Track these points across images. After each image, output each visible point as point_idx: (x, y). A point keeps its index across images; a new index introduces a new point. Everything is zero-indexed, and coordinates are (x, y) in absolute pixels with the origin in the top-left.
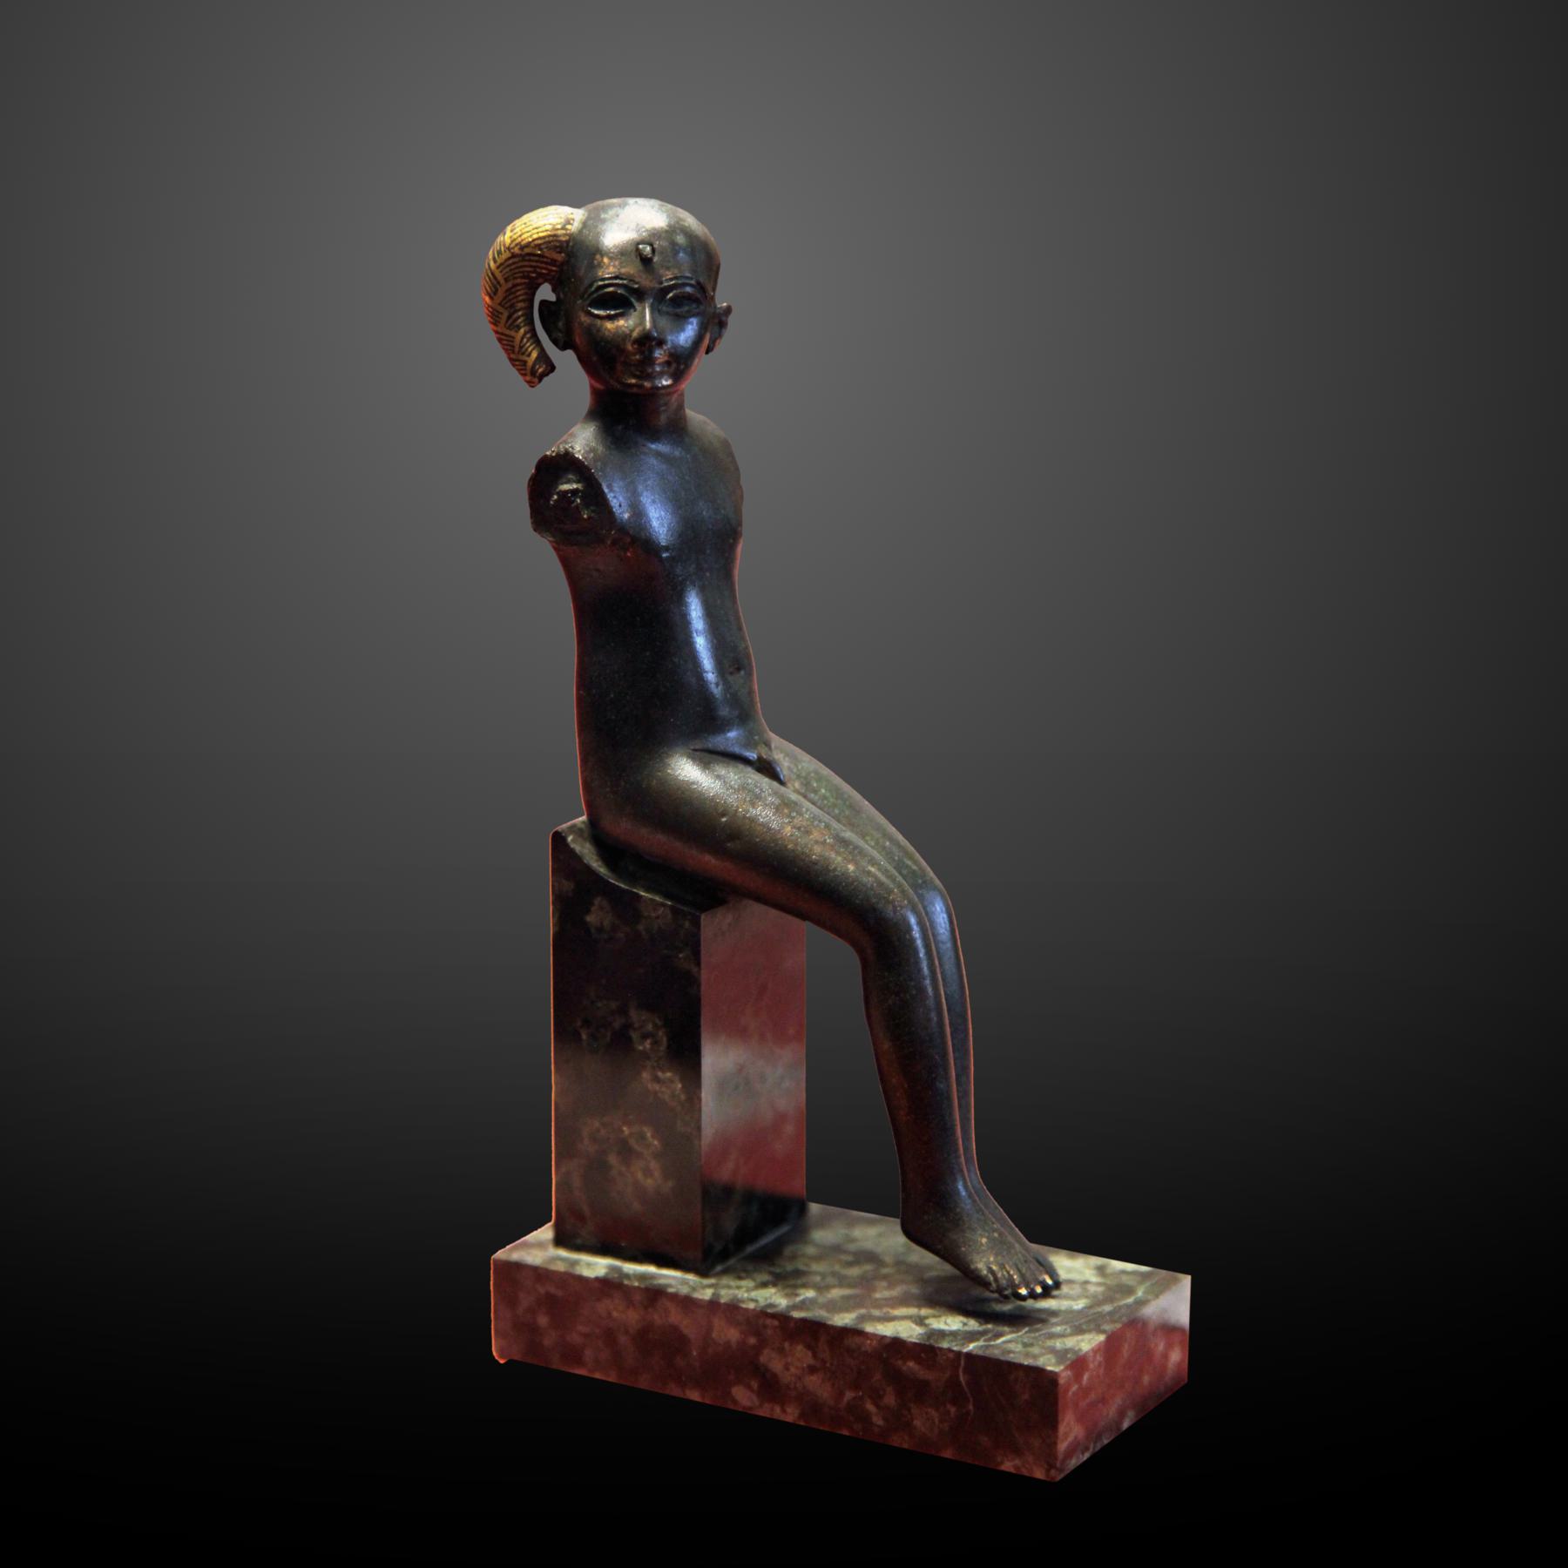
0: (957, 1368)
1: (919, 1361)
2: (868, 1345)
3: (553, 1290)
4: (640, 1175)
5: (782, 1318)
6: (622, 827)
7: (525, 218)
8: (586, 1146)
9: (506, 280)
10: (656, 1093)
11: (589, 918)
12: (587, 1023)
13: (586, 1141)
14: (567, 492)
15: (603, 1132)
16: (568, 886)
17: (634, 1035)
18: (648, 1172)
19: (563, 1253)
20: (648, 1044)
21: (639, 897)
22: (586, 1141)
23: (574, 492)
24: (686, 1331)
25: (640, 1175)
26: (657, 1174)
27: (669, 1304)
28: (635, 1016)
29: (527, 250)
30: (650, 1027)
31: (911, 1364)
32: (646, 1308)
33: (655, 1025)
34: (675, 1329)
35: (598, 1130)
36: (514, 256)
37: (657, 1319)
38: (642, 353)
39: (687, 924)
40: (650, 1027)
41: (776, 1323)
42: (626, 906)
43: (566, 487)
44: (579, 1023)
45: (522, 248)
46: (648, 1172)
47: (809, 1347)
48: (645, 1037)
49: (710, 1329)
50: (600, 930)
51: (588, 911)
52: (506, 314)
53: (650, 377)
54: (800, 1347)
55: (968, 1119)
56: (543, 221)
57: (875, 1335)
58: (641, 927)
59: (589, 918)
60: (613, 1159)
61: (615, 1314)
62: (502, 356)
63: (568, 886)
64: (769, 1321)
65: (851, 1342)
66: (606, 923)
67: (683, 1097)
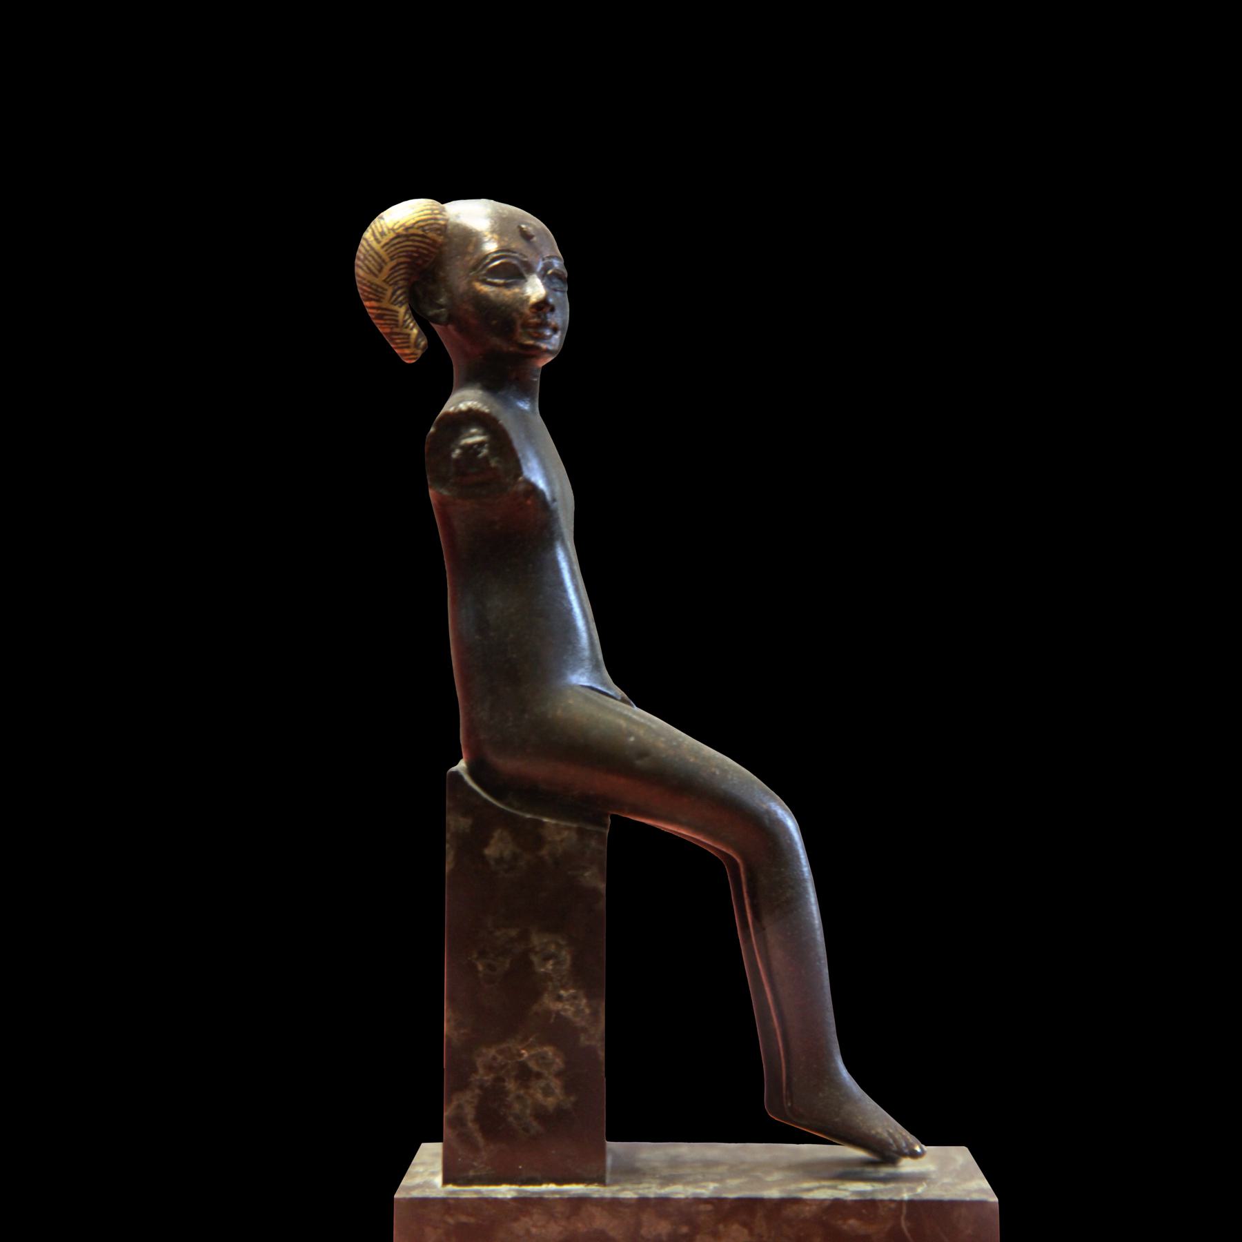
0: (898, 1217)
1: (860, 1217)
2: (807, 1211)
3: (463, 1219)
4: (539, 1096)
5: (717, 1203)
9: (392, 259)
10: (558, 1013)
11: (487, 852)
12: (482, 954)
13: (481, 1071)
14: (471, 446)
15: (500, 1058)
17: (535, 959)
18: (547, 1091)
20: (550, 965)
21: (543, 823)
22: (481, 1071)
23: (481, 444)
24: (612, 1234)
25: (539, 1096)
26: (558, 1091)
27: (594, 1210)
28: (536, 940)
29: (411, 231)
30: (552, 948)
31: (852, 1222)
32: (568, 1218)
33: (558, 945)
34: (602, 1232)
35: (494, 1058)
36: (398, 236)
37: (581, 1227)
38: (539, 317)
40: (552, 948)
41: (709, 1207)
42: (530, 837)
43: (470, 441)
44: (475, 956)
45: (407, 229)
46: (547, 1091)
47: (745, 1225)
48: (546, 959)
49: (639, 1224)
50: (500, 860)
51: (486, 844)
52: (389, 293)
53: (542, 338)
54: (735, 1227)
55: (778, 1017)
57: (814, 1200)
58: (544, 852)
59: (487, 852)
60: (511, 1085)
61: (534, 1230)
64: (702, 1207)
65: (789, 1212)
66: (507, 853)
67: (587, 1011)
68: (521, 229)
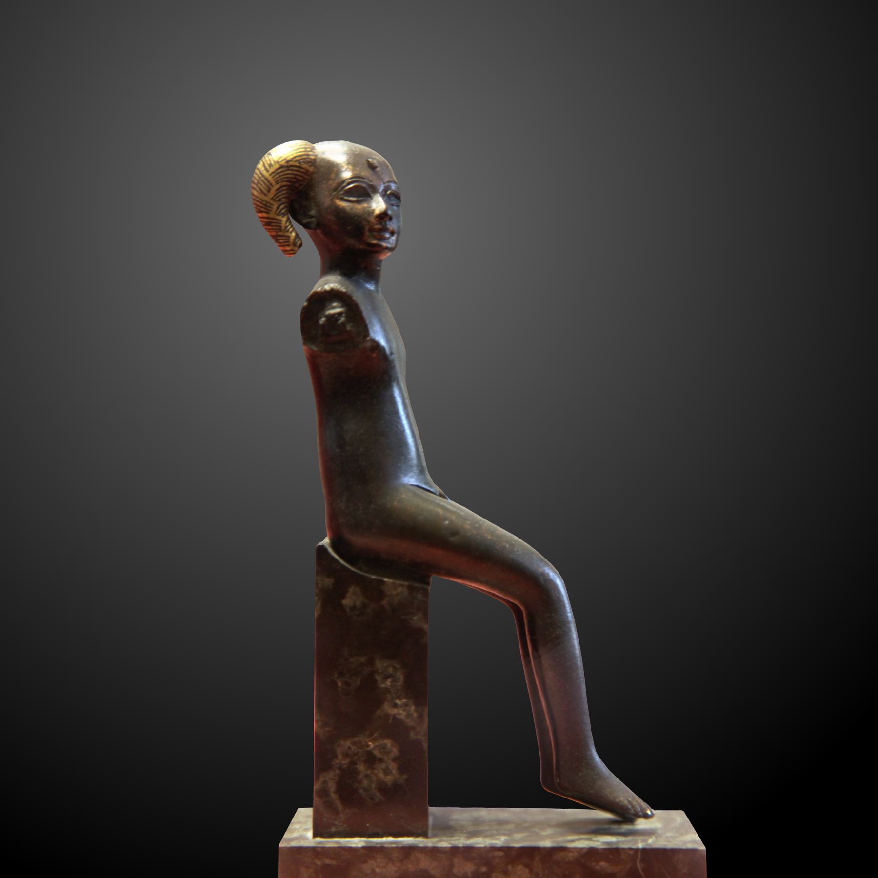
0: (635, 861)
1: (608, 860)
2: (571, 856)
3: (328, 862)
4: (381, 775)
5: (507, 850)
6: (359, 540)
7: (272, 151)
8: (341, 761)
9: (277, 183)
10: (394, 716)
11: (344, 602)
12: (341, 674)
13: (340, 757)
14: (333, 315)
15: (353, 748)
17: (378, 678)
18: (387, 772)
19: (318, 839)
20: (389, 683)
21: (384, 582)
22: (340, 757)
23: (340, 314)
24: (433, 872)
25: (381, 775)
26: (394, 771)
27: (420, 855)
28: (379, 665)
29: (291, 163)
30: (391, 670)
31: (602, 864)
32: (402, 861)
33: (394, 668)
34: (426, 871)
35: (349, 748)
36: (282, 167)
37: (411, 868)
38: (381, 224)
39: (419, 596)
40: (391, 670)
41: (501, 853)
42: (375, 591)
43: (332, 311)
44: (336, 676)
45: (288, 162)
46: (387, 772)
47: (526, 866)
48: (386, 678)
49: (452, 866)
50: (353, 608)
51: (343, 597)
52: (275, 207)
53: (383, 239)
54: (520, 867)
56: (285, 151)
57: (576, 849)
58: (384, 602)
59: (344, 602)
60: (361, 767)
61: (377, 870)
62: (265, 236)
63: (328, 582)
64: (496, 853)
65: (558, 857)
66: (358, 603)
67: (415, 715)
68: (368, 162)
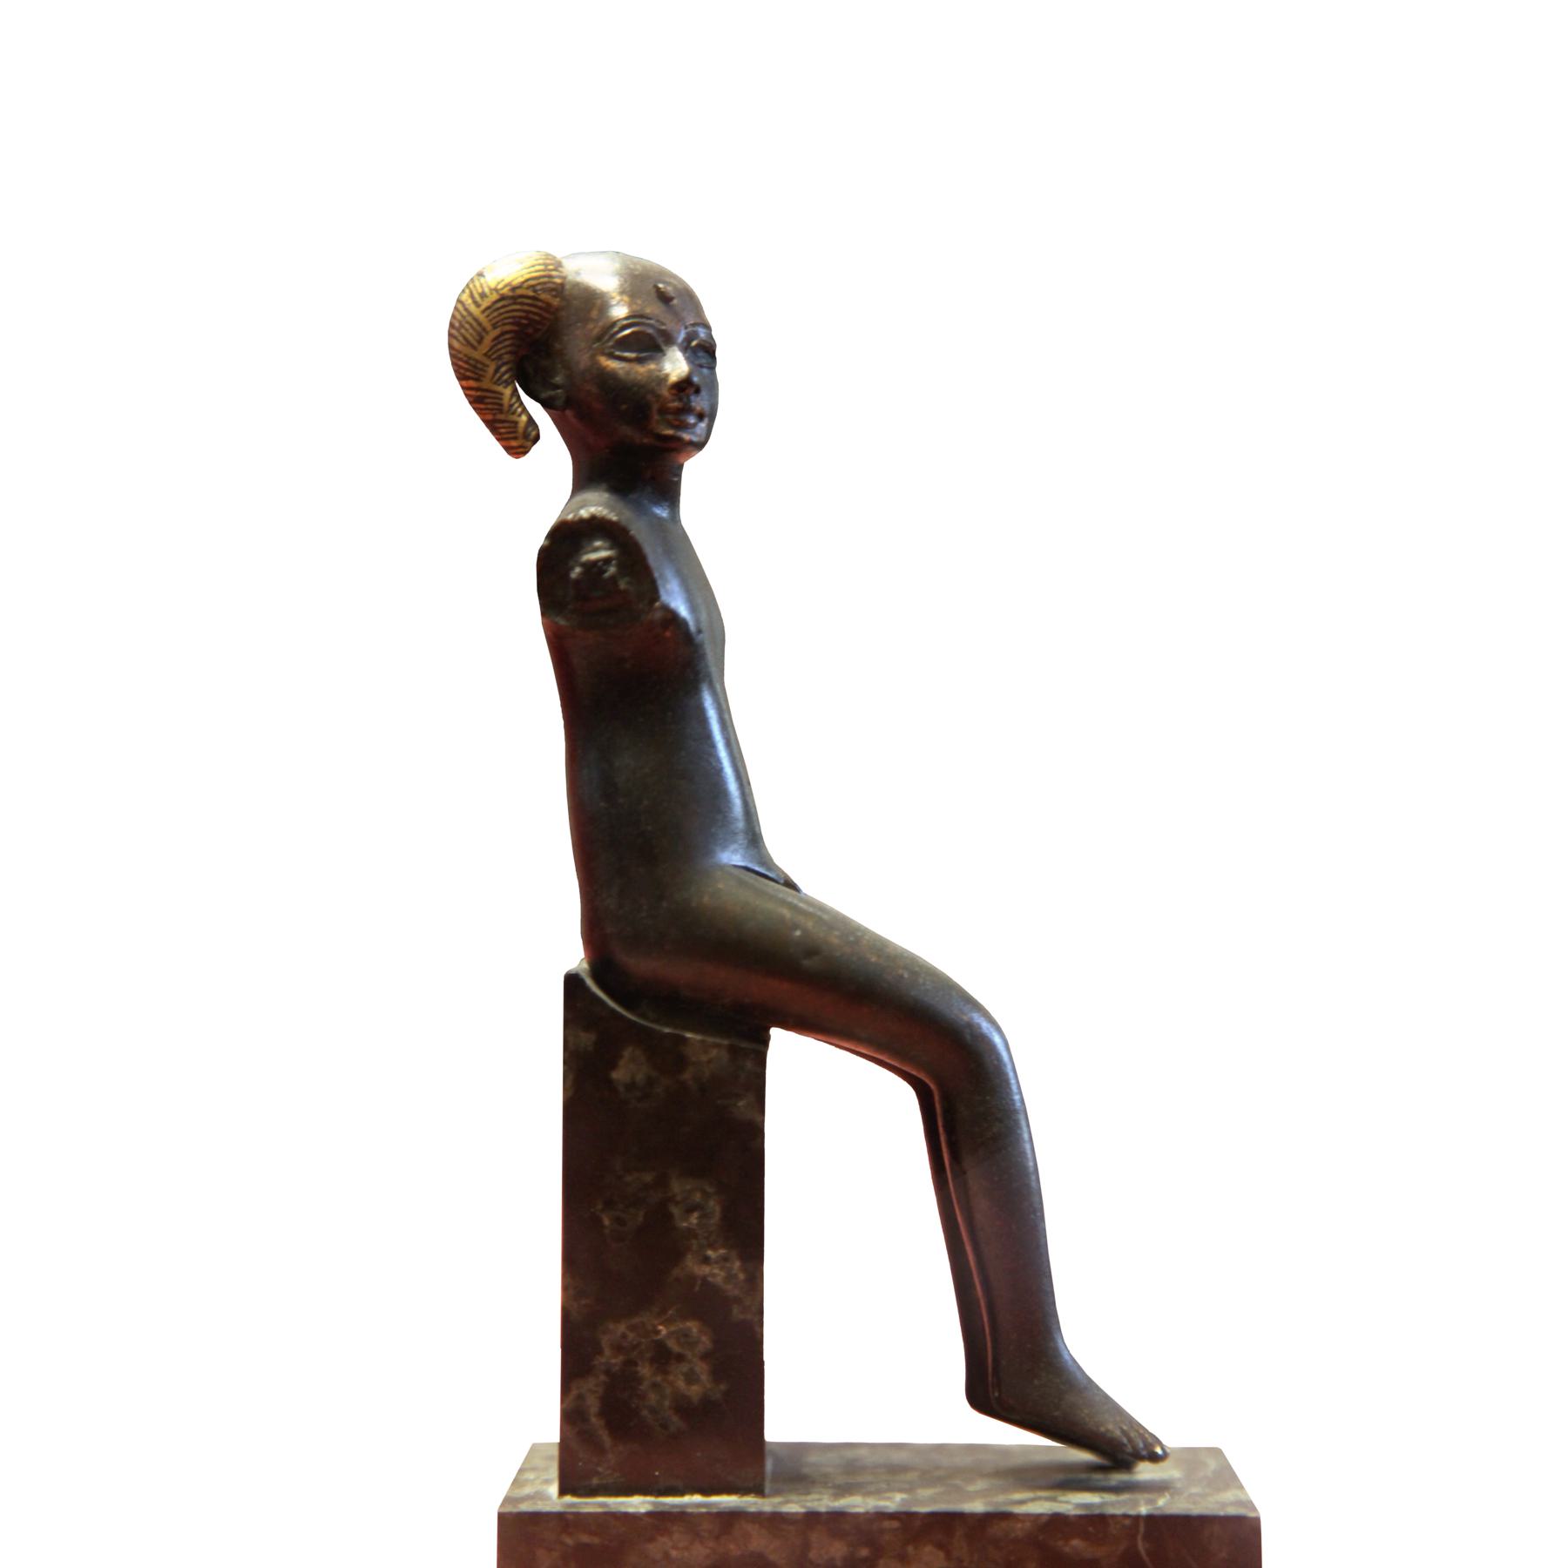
0: (1133, 1537)
1: (1085, 1536)
2: (1019, 1529)
3: (585, 1539)
4: (681, 1384)
5: (905, 1518)
8: (609, 1359)
9: (495, 326)
10: (704, 1279)
11: (615, 1075)
12: (609, 1204)
13: (607, 1352)
14: (594, 563)
15: (631, 1335)
16: (587, 1039)
17: (676, 1211)
18: (691, 1378)
19: (568, 1499)
20: (694, 1219)
21: (685, 1040)
22: (607, 1352)
23: (607, 561)
24: (773, 1557)
25: (681, 1384)
26: (704, 1377)
27: (749, 1527)
28: (677, 1187)
29: (519, 292)
30: (697, 1197)
31: (1076, 1542)
32: (717, 1538)
33: (704, 1193)
34: (761, 1556)
35: (624, 1336)
36: (503, 298)
37: (734, 1549)
38: (680, 400)
40: (697, 1197)
41: (895, 1524)
42: (669, 1056)
43: (593, 556)
44: (600, 1207)
45: (514, 289)
46: (691, 1378)
47: (940, 1546)
48: (690, 1210)
49: (806, 1546)
50: (631, 1086)
51: (613, 1065)
52: (491, 370)
54: (928, 1549)
57: (1028, 1515)
58: (687, 1076)
59: (615, 1075)
60: (645, 1370)
61: (674, 1553)
64: (887, 1524)
65: (996, 1530)
66: (640, 1077)
67: (742, 1276)
68: (658, 289)
